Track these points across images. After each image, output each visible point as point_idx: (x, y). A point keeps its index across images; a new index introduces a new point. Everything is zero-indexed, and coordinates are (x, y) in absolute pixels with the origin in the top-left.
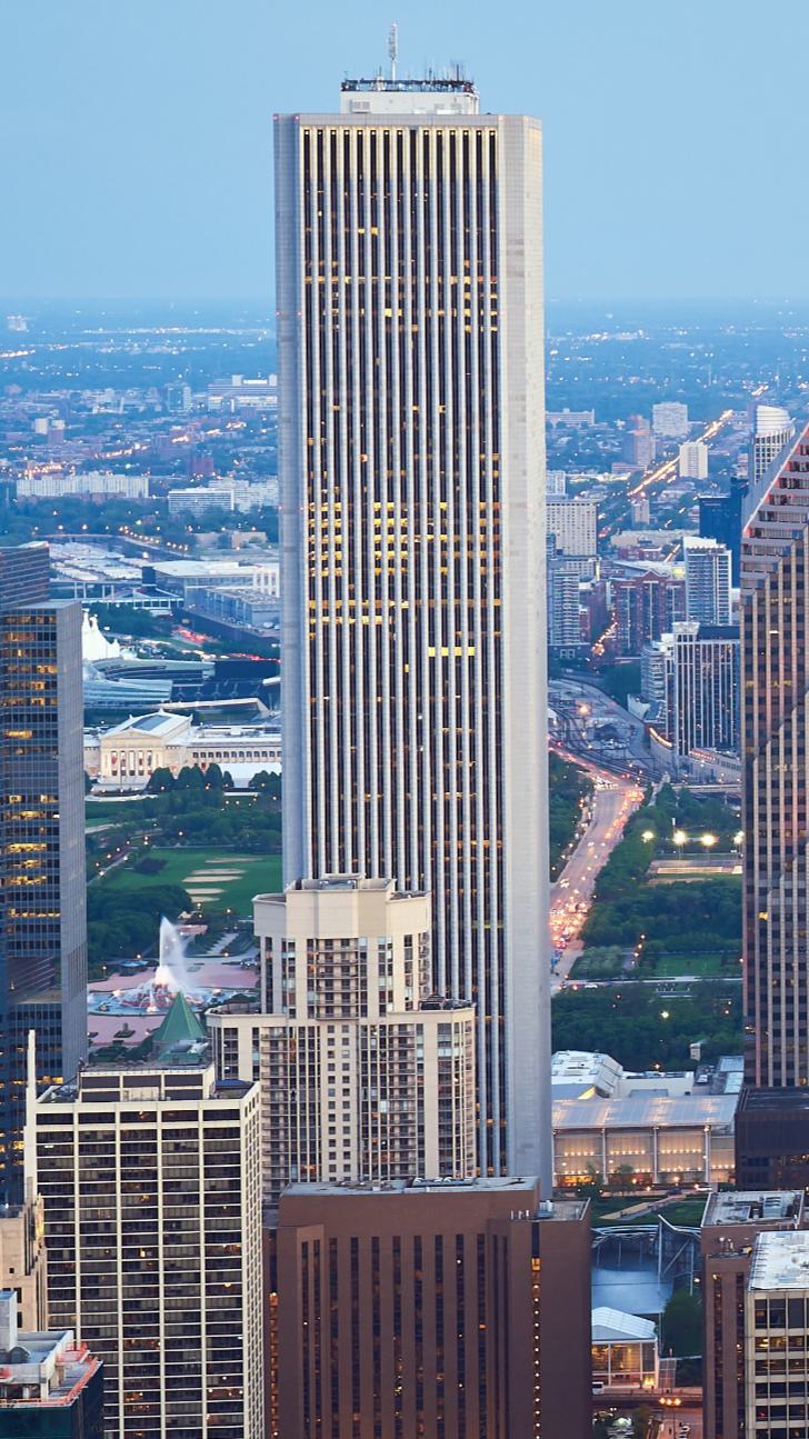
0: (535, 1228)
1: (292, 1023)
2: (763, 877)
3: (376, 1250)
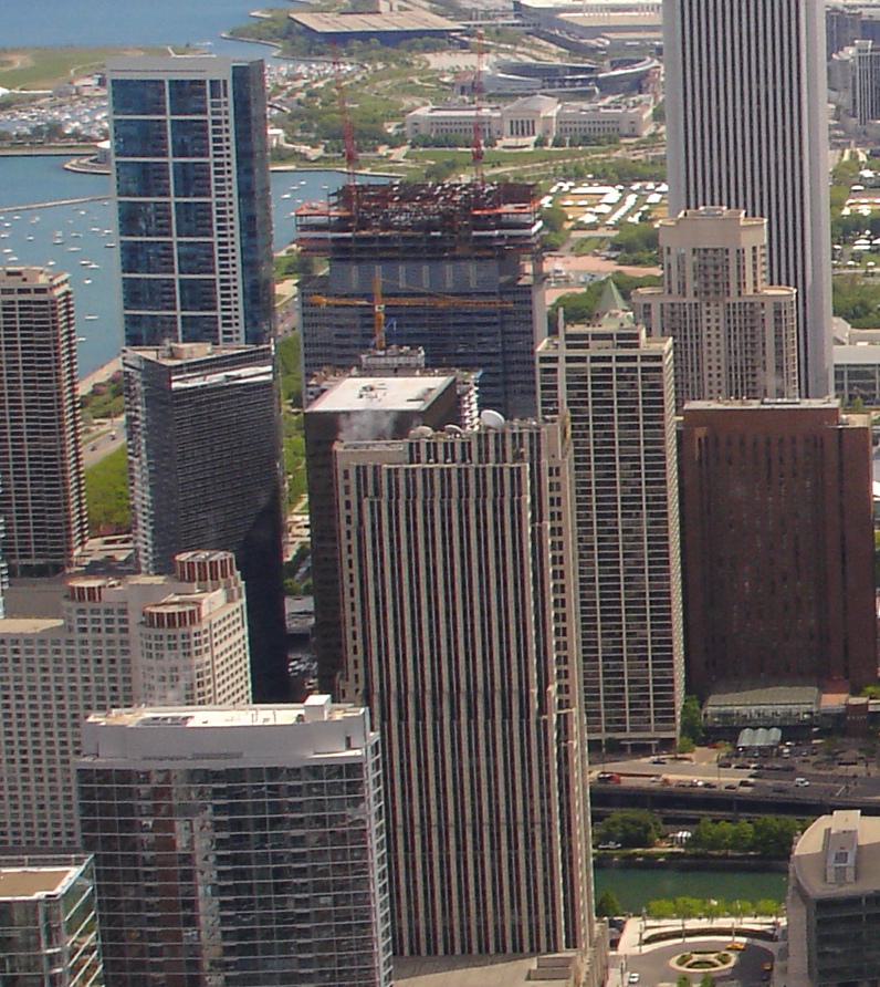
1: (685, 300)
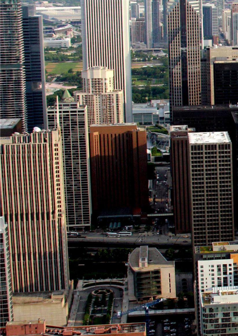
0: (137, 132)
1: (89, 94)
2: (172, 66)
3: (104, 137)
